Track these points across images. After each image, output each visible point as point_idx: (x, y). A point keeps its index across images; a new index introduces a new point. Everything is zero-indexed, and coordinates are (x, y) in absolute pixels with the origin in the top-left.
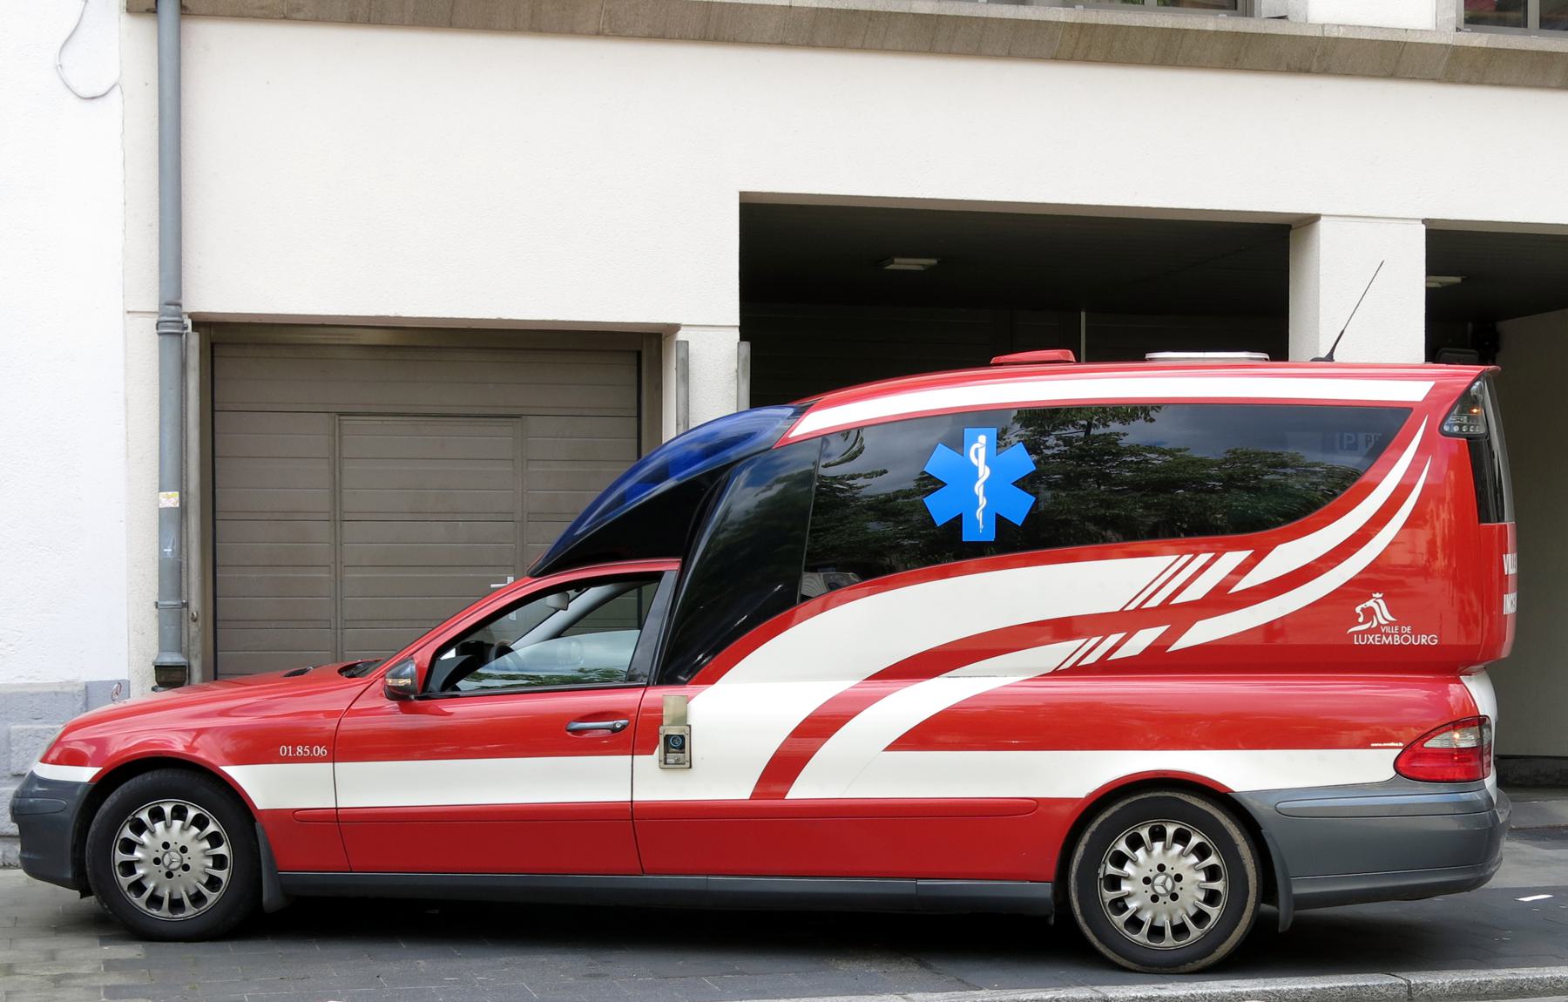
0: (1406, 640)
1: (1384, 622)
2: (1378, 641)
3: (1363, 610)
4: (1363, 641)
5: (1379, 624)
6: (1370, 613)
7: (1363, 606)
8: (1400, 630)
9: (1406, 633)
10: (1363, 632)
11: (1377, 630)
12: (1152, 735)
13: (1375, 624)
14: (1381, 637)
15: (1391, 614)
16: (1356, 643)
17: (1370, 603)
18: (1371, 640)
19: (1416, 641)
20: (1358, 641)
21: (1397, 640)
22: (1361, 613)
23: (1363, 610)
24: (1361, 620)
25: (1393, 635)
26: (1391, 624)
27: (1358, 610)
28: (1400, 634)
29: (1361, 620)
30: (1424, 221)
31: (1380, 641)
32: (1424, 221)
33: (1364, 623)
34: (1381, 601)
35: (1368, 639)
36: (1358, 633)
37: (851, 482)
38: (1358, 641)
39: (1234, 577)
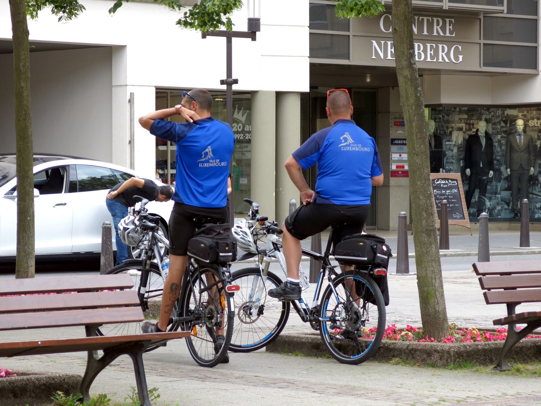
0: (217, 164)
1: (351, 142)
2: (208, 165)
3: (343, 138)
4: (203, 165)
5: (350, 143)
6: (346, 140)
7: (343, 137)
8: (357, 145)
9: (360, 147)
10: (345, 146)
11: (349, 145)
12: (36, 382)
13: (348, 143)
14: (352, 148)
15: (353, 140)
16: (342, 150)
17: (345, 136)
18: (348, 149)
19: (220, 165)
20: (201, 165)
21: (215, 164)
22: (203, 154)
23: (343, 138)
24: (343, 141)
25: (213, 163)
26: (353, 143)
27: (341, 138)
28: (216, 162)
29: (203, 157)
30: (155, 87)
31: (352, 149)
32: (155, 87)
33: (204, 158)
34: (348, 135)
35: (347, 148)
36: (343, 146)
37: (421, 400)
38: (201, 165)
39: (207, 120)
